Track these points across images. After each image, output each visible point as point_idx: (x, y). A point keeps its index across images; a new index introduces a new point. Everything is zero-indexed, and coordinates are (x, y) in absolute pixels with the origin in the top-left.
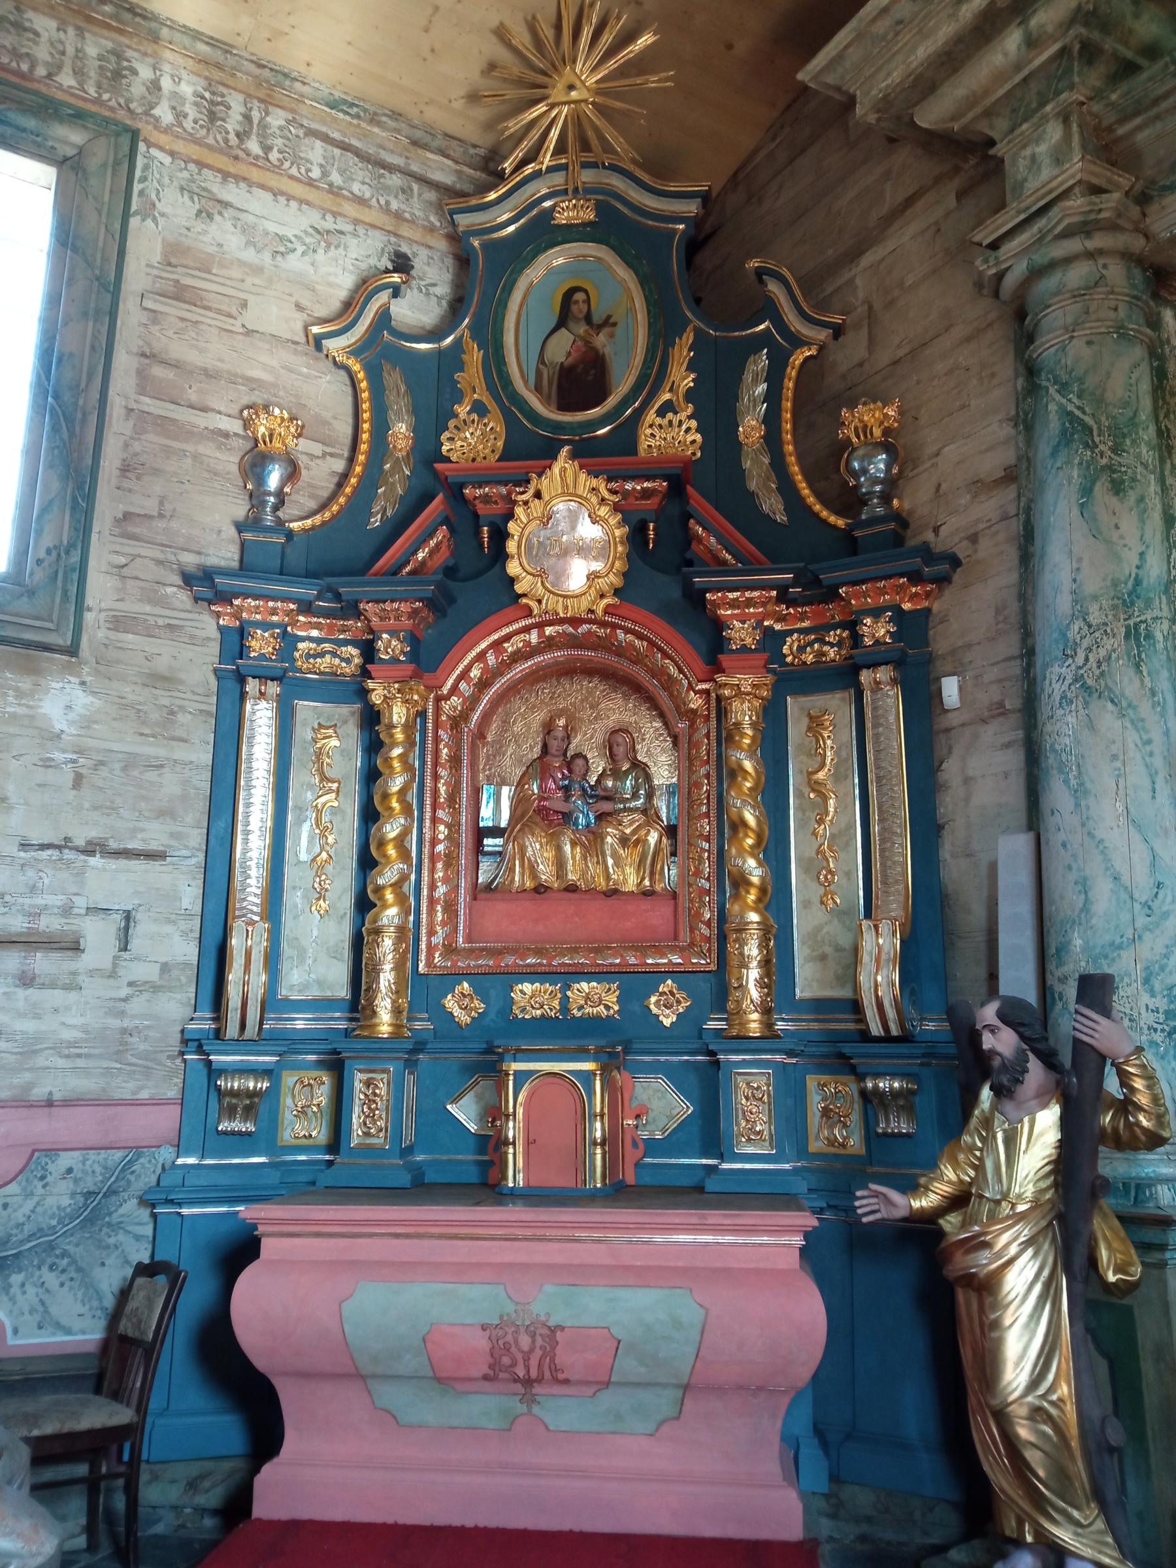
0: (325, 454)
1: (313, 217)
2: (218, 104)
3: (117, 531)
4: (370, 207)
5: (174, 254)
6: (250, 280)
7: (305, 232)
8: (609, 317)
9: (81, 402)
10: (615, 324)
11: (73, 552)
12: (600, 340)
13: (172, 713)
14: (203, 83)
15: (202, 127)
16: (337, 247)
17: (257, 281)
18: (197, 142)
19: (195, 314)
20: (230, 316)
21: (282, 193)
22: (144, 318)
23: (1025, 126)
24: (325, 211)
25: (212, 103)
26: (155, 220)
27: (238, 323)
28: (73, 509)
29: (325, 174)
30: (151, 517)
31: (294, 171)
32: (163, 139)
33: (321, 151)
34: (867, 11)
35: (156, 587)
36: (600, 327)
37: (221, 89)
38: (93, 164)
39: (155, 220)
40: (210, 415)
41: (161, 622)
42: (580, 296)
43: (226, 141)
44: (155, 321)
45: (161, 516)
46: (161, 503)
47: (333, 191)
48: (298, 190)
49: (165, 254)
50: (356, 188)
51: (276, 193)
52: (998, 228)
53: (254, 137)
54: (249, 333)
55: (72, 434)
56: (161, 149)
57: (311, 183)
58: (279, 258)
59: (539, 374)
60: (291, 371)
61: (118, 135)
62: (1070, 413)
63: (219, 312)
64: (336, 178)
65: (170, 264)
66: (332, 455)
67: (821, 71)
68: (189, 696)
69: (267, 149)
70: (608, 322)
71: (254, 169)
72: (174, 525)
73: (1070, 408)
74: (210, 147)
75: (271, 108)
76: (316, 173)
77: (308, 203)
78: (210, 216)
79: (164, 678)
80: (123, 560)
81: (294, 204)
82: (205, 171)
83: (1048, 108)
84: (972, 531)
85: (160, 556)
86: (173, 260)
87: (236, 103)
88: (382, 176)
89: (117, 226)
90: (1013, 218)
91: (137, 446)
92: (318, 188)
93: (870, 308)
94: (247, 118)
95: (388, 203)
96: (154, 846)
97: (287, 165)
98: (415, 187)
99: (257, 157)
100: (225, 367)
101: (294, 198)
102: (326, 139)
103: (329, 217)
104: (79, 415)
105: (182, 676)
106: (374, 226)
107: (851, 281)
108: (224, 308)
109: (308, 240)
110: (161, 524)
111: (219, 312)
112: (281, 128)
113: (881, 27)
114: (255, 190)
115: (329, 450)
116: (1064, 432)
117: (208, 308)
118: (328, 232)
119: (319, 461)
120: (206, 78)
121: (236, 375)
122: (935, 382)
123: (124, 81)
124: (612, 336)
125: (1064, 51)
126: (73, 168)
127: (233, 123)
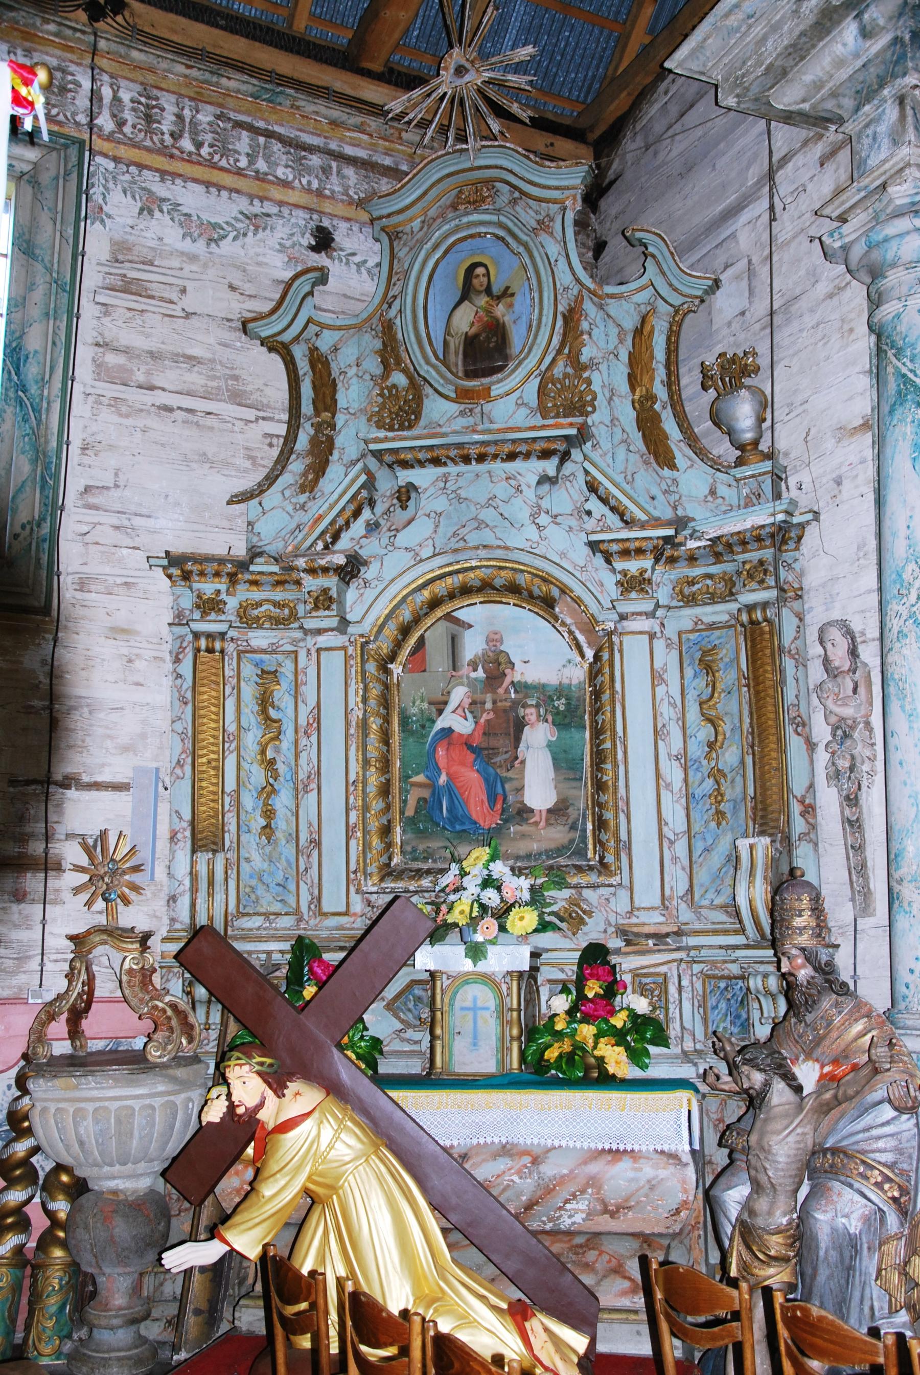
0: (257, 420)
1: (243, 203)
2: (154, 107)
3: (79, 503)
4: (293, 188)
5: (120, 252)
6: (188, 268)
7: (236, 219)
8: (508, 288)
9: (46, 392)
10: (513, 295)
11: (43, 525)
12: (500, 310)
13: (130, 661)
14: (139, 88)
15: (140, 131)
16: (264, 229)
17: (194, 268)
18: (136, 146)
19: (142, 303)
20: (172, 302)
21: (214, 185)
22: (97, 310)
23: (867, 108)
24: (251, 197)
25: (148, 106)
26: (102, 221)
27: (178, 308)
28: (42, 488)
29: (251, 163)
30: (108, 488)
31: (224, 163)
32: (106, 146)
33: (247, 140)
34: (720, 9)
35: (113, 550)
36: (499, 298)
37: (155, 92)
38: (45, 178)
39: (102, 221)
40: (157, 392)
41: (119, 581)
42: (480, 271)
43: (162, 141)
44: (106, 314)
45: (117, 486)
46: (116, 475)
47: (260, 177)
48: (228, 180)
49: (113, 253)
50: (280, 172)
51: (208, 184)
52: (843, 203)
53: (186, 135)
54: (188, 315)
55: (39, 422)
56: (106, 156)
57: (239, 172)
58: (213, 245)
59: (446, 344)
60: (225, 345)
61: (66, 147)
62: (904, 376)
63: (162, 299)
64: (261, 165)
65: (117, 261)
66: (264, 419)
67: (684, 60)
68: (144, 645)
69: (199, 145)
70: (507, 293)
71: (188, 165)
72: (127, 493)
73: (904, 370)
74: (148, 150)
75: (201, 105)
76: (243, 162)
77: (238, 191)
78: (151, 212)
79: (124, 631)
80: (85, 529)
81: (224, 194)
82: (145, 172)
83: (886, 92)
84: (837, 473)
85: (116, 522)
86: (120, 257)
87: (168, 103)
88: (304, 158)
89: (71, 231)
90: (854, 195)
91: (94, 428)
92: (245, 176)
93: (750, 262)
94: (180, 117)
95: (309, 183)
96: (120, 779)
97: (217, 158)
98: (334, 164)
99: (190, 153)
100: (169, 348)
101: (224, 188)
102: (251, 128)
103: (256, 202)
104: (45, 405)
105: (138, 627)
106: (297, 206)
107: (733, 236)
108: (166, 295)
109: (239, 225)
110: (115, 493)
111: (162, 299)
112: (210, 124)
113: (733, 21)
114: (190, 185)
115: (261, 414)
116: (899, 393)
117: (152, 297)
118: (256, 216)
119: (253, 425)
120: (142, 84)
121: (177, 355)
122: (804, 334)
123: (70, 95)
124: (511, 305)
125: (896, 40)
126: (29, 182)
127: (167, 125)
